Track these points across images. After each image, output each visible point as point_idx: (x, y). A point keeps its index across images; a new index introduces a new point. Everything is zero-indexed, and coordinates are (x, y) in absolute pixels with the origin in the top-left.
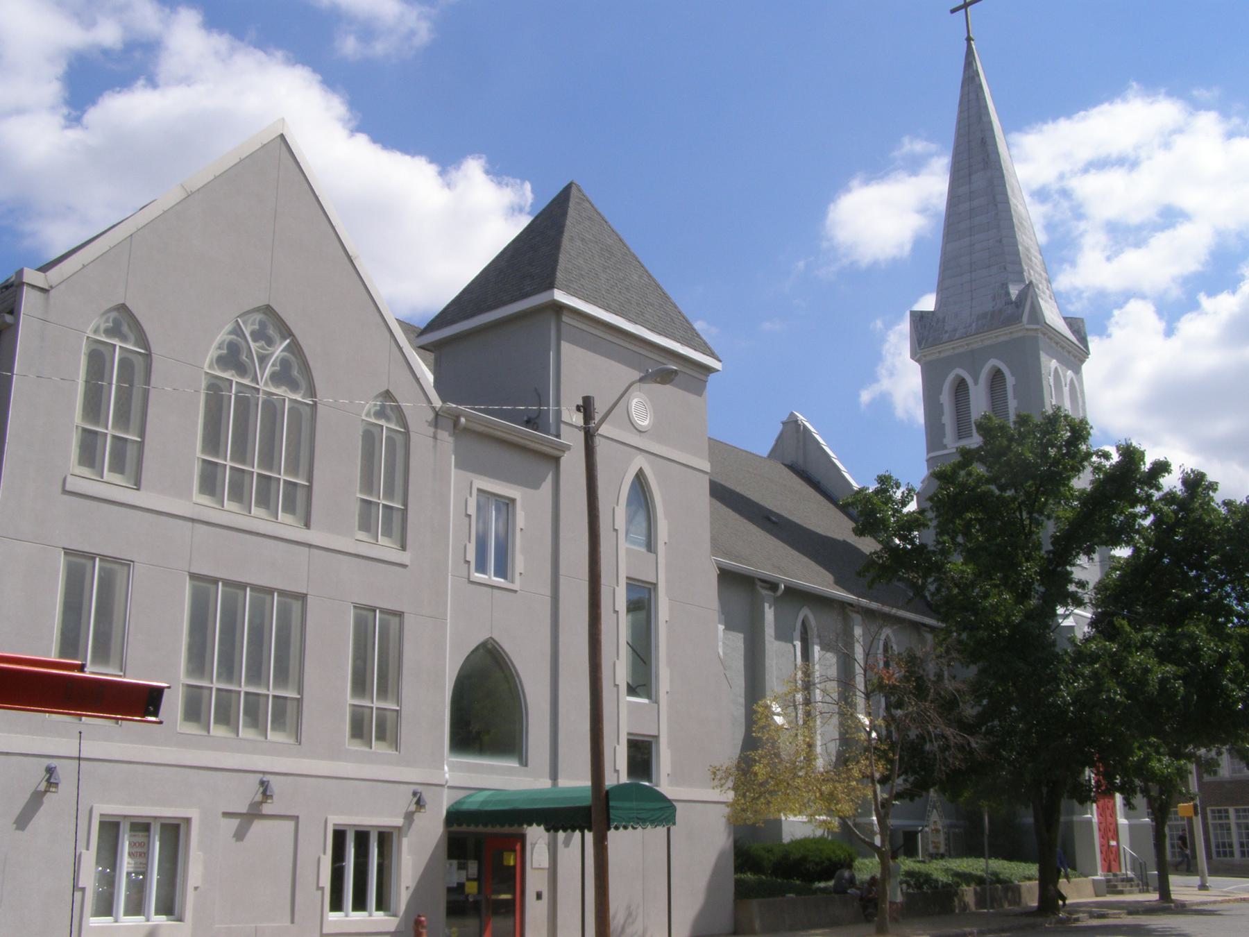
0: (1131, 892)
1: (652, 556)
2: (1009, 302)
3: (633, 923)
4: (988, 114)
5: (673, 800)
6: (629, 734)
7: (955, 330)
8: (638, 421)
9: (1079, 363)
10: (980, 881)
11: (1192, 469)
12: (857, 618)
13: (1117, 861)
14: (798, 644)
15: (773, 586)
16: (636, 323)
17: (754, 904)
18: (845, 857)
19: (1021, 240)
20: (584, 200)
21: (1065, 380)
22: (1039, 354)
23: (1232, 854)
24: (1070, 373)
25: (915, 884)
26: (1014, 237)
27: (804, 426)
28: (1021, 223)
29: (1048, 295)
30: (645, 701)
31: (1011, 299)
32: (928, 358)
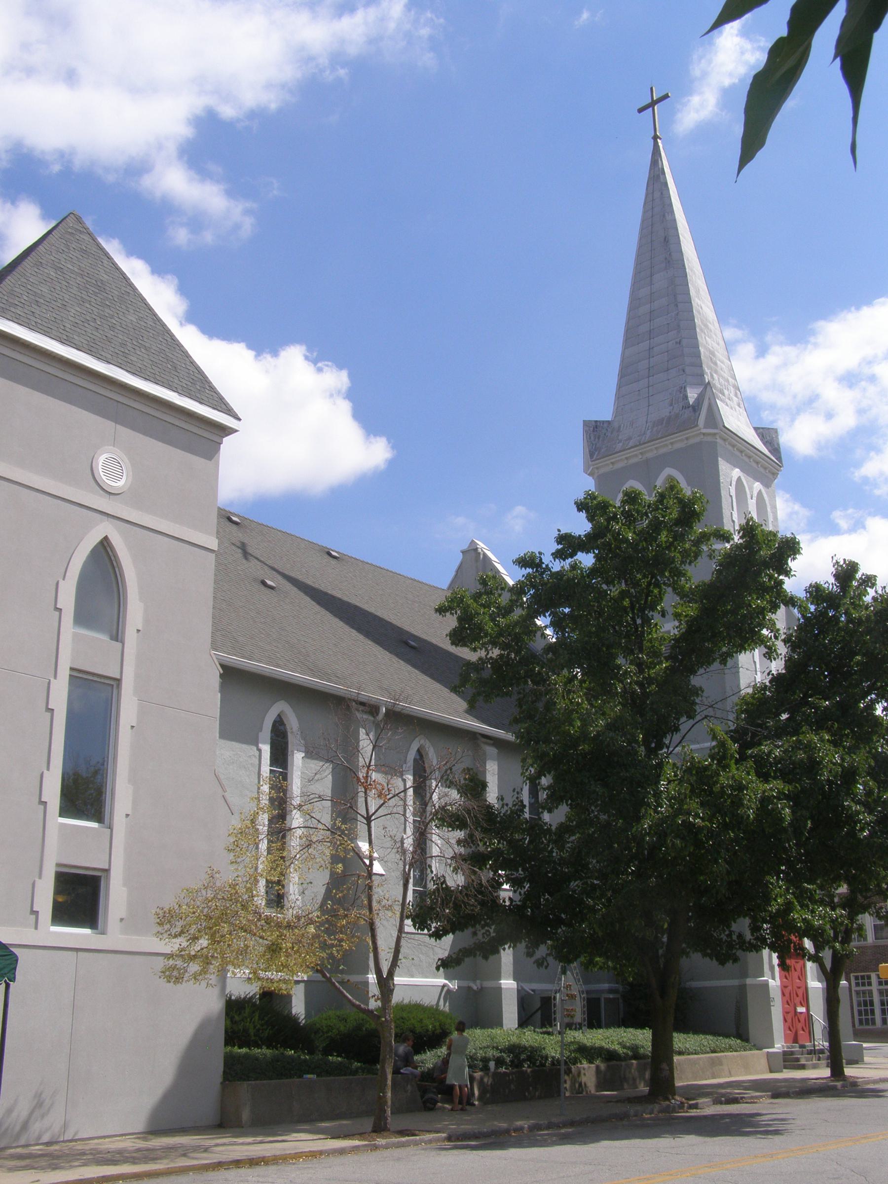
0: (815, 1067)
1: (119, 645)
2: (687, 406)
3: (43, 1116)
4: (672, 212)
5: (10, 944)
6: (58, 865)
7: (630, 439)
8: (104, 478)
9: (771, 476)
10: (610, 1056)
11: (845, 560)
12: (491, 750)
13: (807, 1031)
14: (266, 749)
15: (372, 709)
16: (109, 363)
17: (244, 1089)
18: (434, 1027)
19: (704, 342)
20: (81, 232)
21: (752, 492)
22: (717, 461)
23: (873, 1022)
24: (757, 486)
25: (512, 1061)
26: (695, 337)
27: (485, 554)
28: (706, 326)
29: (735, 403)
30: (94, 825)
31: (689, 402)
32: (602, 471)
